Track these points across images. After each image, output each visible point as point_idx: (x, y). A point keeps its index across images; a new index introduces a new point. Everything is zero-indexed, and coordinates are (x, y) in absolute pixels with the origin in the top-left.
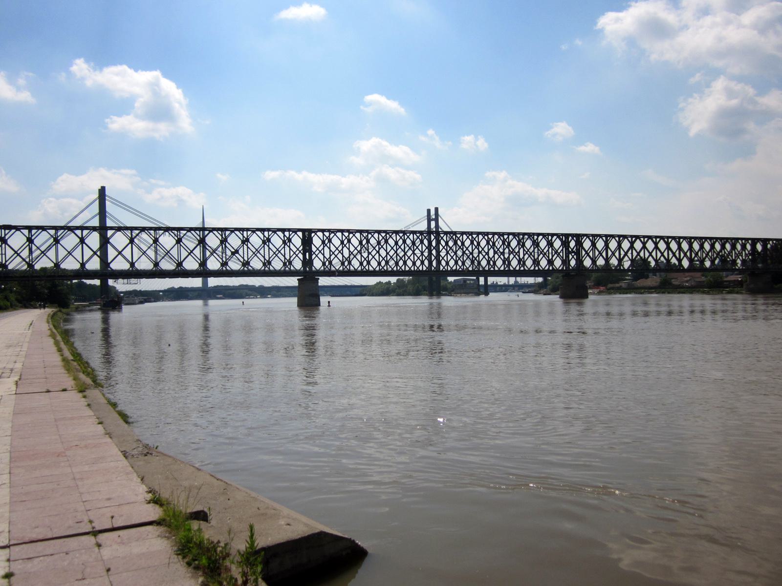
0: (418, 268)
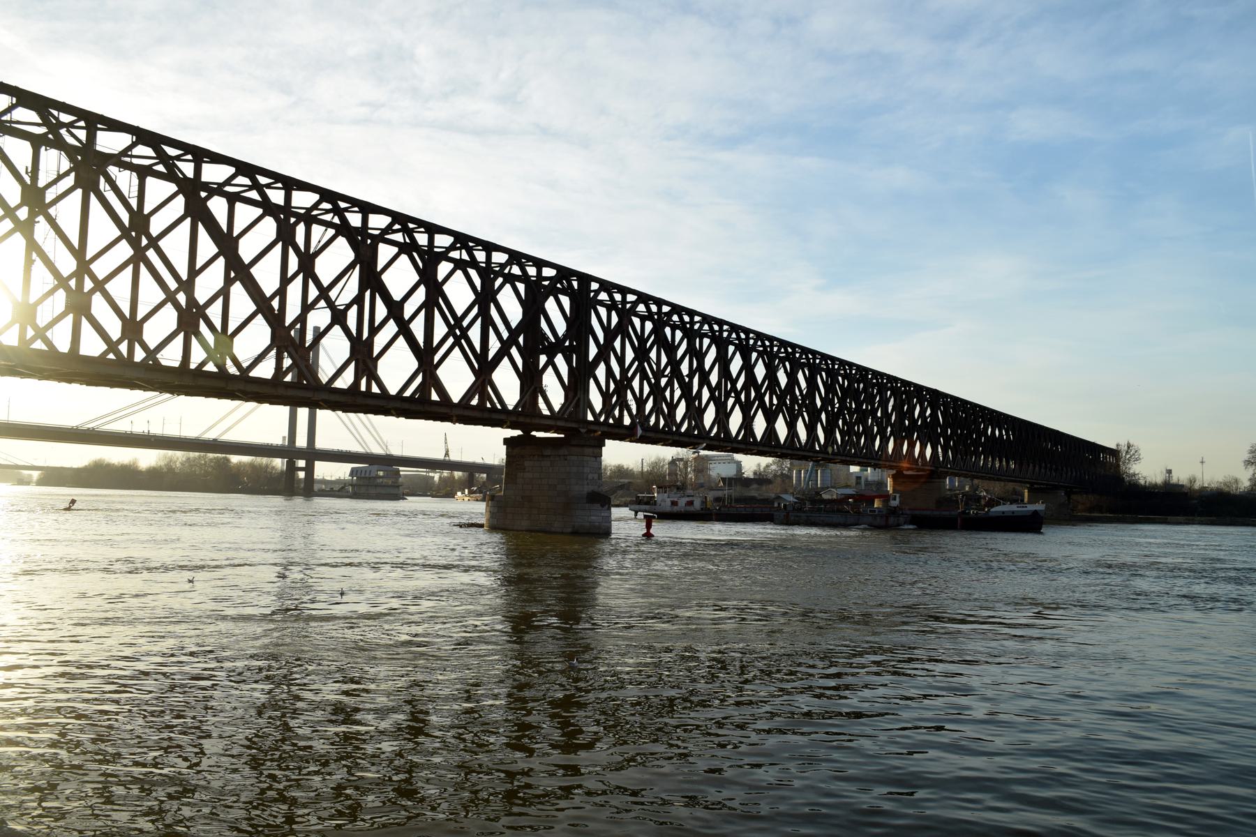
0: (151, 354)
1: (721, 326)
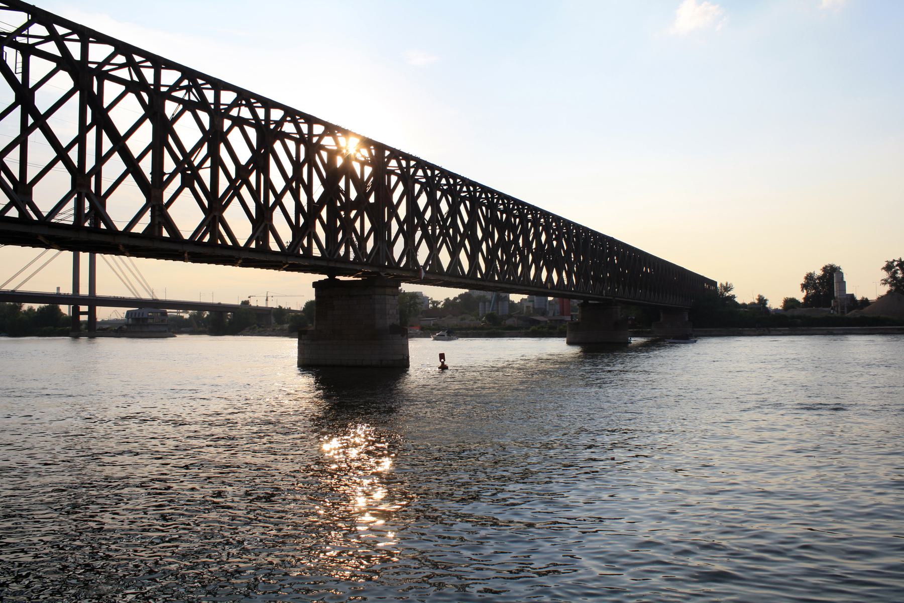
1: (474, 186)
